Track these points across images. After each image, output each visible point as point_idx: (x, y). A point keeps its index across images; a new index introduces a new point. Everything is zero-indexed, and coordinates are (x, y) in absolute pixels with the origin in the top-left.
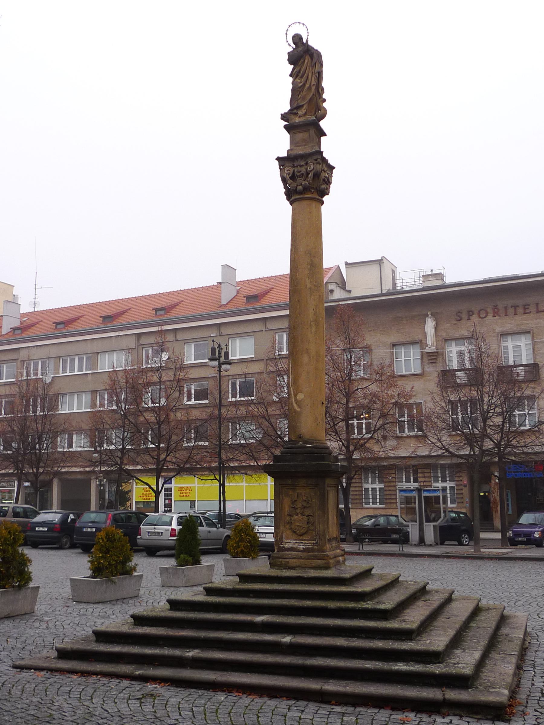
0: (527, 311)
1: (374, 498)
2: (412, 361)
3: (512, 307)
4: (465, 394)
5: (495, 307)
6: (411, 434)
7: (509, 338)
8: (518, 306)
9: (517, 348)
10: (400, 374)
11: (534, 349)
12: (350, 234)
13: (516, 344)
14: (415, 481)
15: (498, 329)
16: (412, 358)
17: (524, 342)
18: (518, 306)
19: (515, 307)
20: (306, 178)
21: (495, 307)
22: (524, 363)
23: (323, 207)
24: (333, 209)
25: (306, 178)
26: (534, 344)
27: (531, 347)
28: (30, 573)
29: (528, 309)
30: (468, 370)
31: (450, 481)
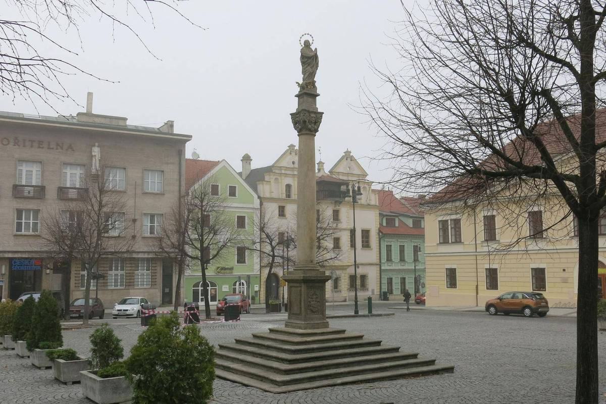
0: (41, 146)
1: (116, 281)
2: (150, 183)
3: (29, 141)
4: (73, 206)
5: (16, 138)
6: (27, 233)
7: (24, 165)
8: (34, 141)
9: (29, 173)
10: (147, 191)
11: (42, 175)
12: (328, 151)
13: (29, 169)
14: (122, 269)
15: (17, 156)
16: (150, 181)
17: (35, 169)
18: (34, 141)
19: (32, 141)
20: (307, 121)
21: (16, 138)
22: (34, 184)
23: (315, 137)
24: (320, 138)
25: (307, 121)
26: (43, 172)
27: (40, 173)
28: (118, 341)
29: (41, 144)
30: (78, 188)
31: (121, 270)
